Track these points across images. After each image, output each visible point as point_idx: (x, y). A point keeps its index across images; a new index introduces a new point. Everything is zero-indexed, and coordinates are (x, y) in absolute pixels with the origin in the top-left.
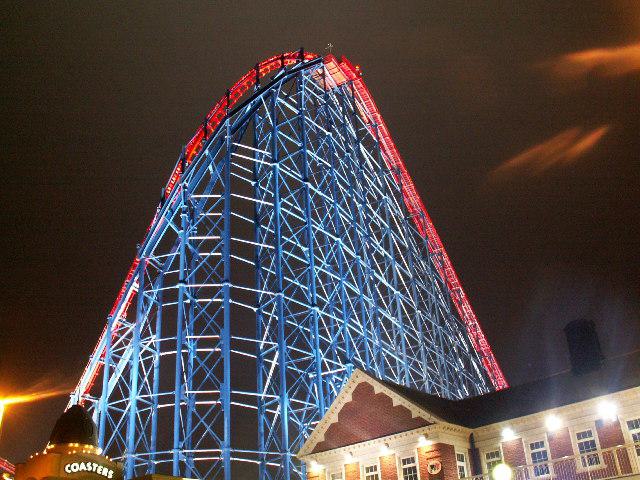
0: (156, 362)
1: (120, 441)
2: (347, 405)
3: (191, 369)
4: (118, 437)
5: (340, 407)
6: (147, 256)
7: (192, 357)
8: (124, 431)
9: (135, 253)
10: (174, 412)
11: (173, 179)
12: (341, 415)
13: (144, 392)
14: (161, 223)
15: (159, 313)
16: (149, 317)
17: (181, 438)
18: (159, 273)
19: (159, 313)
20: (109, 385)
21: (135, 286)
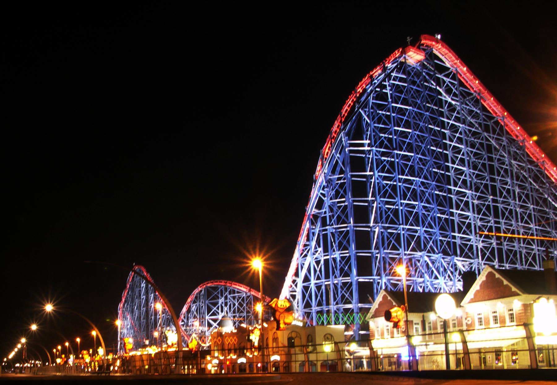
0: (322, 262)
1: (318, 320)
2: (381, 302)
3: (338, 266)
4: (319, 321)
5: (378, 303)
6: (311, 209)
7: (338, 259)
8: (310, 296)
9: (305, 211)
10: (344, 220)
11: (318, 168)
12: (379, 305)
13: (318, 278)
14: (315, 193)
15: (321, 237)
16: (316, 241)
17: (335, 299)
18: (319, 216)
19: (321, 237)
20: (302, 274)
21: (308, 225)
